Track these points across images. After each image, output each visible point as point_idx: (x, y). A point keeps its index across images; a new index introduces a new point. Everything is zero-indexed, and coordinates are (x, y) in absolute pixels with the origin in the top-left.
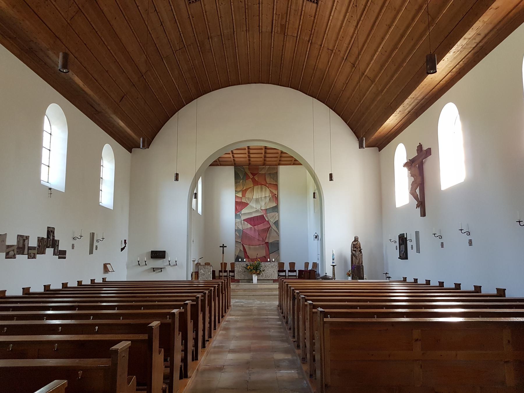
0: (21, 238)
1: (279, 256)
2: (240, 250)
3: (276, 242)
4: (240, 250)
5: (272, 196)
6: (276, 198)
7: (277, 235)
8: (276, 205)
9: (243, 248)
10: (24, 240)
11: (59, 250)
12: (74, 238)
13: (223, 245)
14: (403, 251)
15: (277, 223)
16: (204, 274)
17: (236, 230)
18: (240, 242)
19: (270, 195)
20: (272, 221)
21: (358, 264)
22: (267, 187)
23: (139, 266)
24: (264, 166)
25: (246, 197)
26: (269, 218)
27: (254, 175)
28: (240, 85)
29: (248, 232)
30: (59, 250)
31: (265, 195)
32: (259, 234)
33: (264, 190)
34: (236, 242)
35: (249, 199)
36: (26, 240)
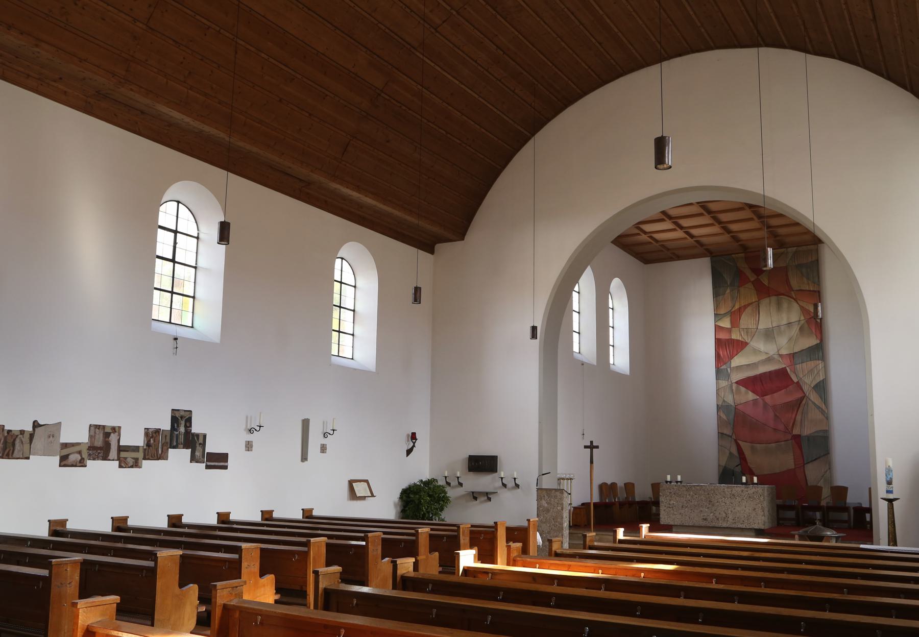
0: (97, 430)
1: (830, 469)
2: (730, 453)
4: (730, 453)
5: (808, 321)
8: (819, 342)
9: (738, 449)
10: (107, 435)
11: (207, 453)
12: (250, 431)
13: (592, 442)
15: (822, 388)
16: (548, 511)
18: (729, 436)
19: (802, 318)
20: (808, 382)
23: (505, 489)
25: (742, 326)
26: (801, 376)
30: (207, 451)
32: (776, 415)
33: (785, 305)
34: (721, 435)
35: (747, 332)
36: (112, 434)
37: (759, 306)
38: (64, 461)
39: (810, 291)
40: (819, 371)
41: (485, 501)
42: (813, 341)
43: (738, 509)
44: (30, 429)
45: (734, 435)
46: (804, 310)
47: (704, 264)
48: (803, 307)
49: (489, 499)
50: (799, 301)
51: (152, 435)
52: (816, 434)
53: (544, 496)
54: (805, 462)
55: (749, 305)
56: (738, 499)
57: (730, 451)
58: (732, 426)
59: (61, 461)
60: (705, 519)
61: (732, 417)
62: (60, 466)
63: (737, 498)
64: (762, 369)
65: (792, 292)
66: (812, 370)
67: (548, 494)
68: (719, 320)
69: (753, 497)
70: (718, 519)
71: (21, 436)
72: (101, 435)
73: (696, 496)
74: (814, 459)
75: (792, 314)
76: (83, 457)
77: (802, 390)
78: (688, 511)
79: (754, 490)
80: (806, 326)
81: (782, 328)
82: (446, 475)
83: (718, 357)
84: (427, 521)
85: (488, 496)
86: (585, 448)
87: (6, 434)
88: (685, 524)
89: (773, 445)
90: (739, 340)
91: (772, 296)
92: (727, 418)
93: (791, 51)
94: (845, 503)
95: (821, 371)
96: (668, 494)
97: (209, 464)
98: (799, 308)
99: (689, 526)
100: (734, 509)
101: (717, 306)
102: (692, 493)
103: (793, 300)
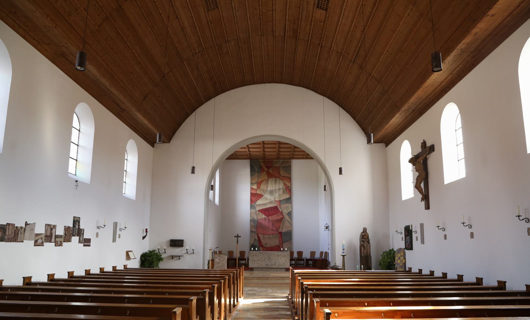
1: (292, 245)
2: (255, 239)
6: (289, 190)
10: (52, 229)
11: (84, 239)
15: (290, 214)
16: (219, 263)
17: (251, 220)
18: (254, 232)
19: (284, 187)
20: (285, 212)
22: (281, 179)
24: (278, 160)
27: (268, 168)
29: (263, 222)
30: (84, 238)
32: (273, 224)
33: (278, 182)
34: (251, 232)
35: (263, 191)
36: (53, 229)
38: (36, 244)
41: (178, 259)
42: (288, 196)
43: (280, 260)
44: (24, 226)
46: (285, 184)
47: (247, 162)
49: (180, 259)
51: (67, 229)
52: (287, 232)
53: (217, 257)
56: (280, 257)
58: (256, 228)
59: (35, 243)
61: (256, 224)
62: (35, 246)
65: (281, 177)
70: (272, 265)
71: (21, 230)
72: (50, 229)
75: (280, 185)
76: (43, 241)
77: (283, 214)
79: (286, 253)
80: (285, 190)
81: (277, 190)
82: (159, 248)
83: (251, 200)
84: (149, 268)
85: (179, 257)
86: (424, 243)
87: (15, 229)
89: (272, 235)
90: (260, 194)
93: (311, 91)
96: (252, 255)
97: (85, 244)
99: (260, 268)
101: (252, 180)
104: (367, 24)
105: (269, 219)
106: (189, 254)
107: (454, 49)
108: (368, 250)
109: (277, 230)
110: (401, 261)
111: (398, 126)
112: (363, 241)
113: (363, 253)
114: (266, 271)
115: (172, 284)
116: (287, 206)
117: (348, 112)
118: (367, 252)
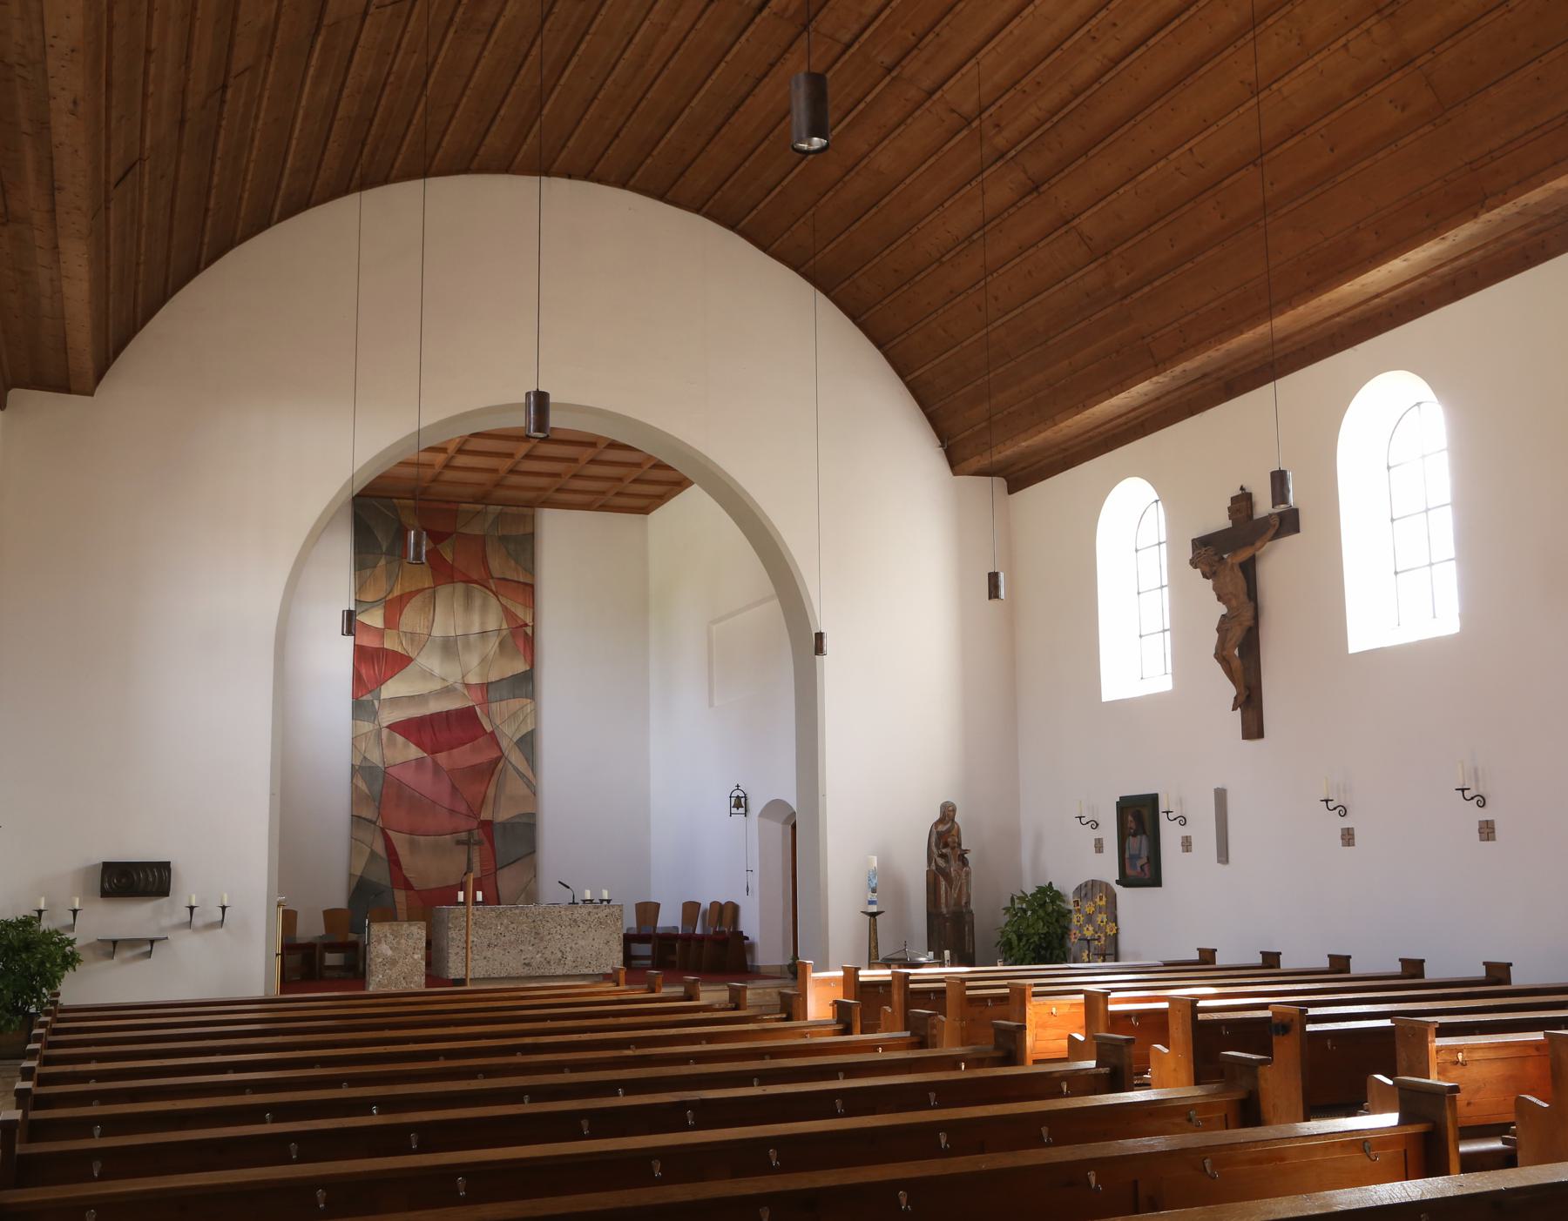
1: (535, 876)
2: (373, 854)
3: (524, 820)
6: (523, 639)
7: (526, 791)
8: (528, 668)
14: (1139, 857)
15: (528, 744)
16: (394, 962)
17: (354, 770)
18: (371, 821)
19: (505, 626)
20: (509, 733)
21: (955, 905)
22: (491, 591)
24: (479, 507)
25: (403, 628)
26: (498, 722)
27: (437, 537)
28: (732, 233)
29: (408, 777)
31: (483, 623)
32: (453, 787)
33: (477, 602)
34: (357, 820)
35: (412, 641)
37: (435, 598)
39: (519, 582)
40: (527, 714)
42: (520, 666)
43: (581, 943)
45: (380, 820)
46: (508, 614)
48: (506, 608)
50: (500, 597)
52: (517, 820)
53: (386, 936)
54: (498, 867)
55: (418, 592)
56: (583, 927)
57: (371, 848)
58: (377, 804)
60: (528, 965)
63: (581, 925)
64: (435, 707)
65: (491, 581)
66: (515, 713)
67: (393, 930)
68: (363, 612)
69: (606, 922)
70: (549, 962)
73: (513, 926)
74: (512, 860)
75: (485, 617)
77: (498, 744)
78: (499, 953)
81: (472, 638)
83: (358, 679)
85: (146, 946)
88: (492, 976)
91: (457, 582)
92: (369, 790)
94: (655, 927)
95: (529, 716)
98: (500, 609)
100: (576, 944)
102: (505, 921)
103: (492, 595)
104: (1149, 38)
105: (435, 763)
106: (196, 930)
107: (1504, 202)
108: (960, 887)
109: (473, 813)
110: (1098, 929)
111: (1112, 420)
112: (943, 856)
113: (943, 900)
114: (673, 995)
115: (98, 1081)
116: (518, 707)
117: (879, 344)
118: (958, 902)
